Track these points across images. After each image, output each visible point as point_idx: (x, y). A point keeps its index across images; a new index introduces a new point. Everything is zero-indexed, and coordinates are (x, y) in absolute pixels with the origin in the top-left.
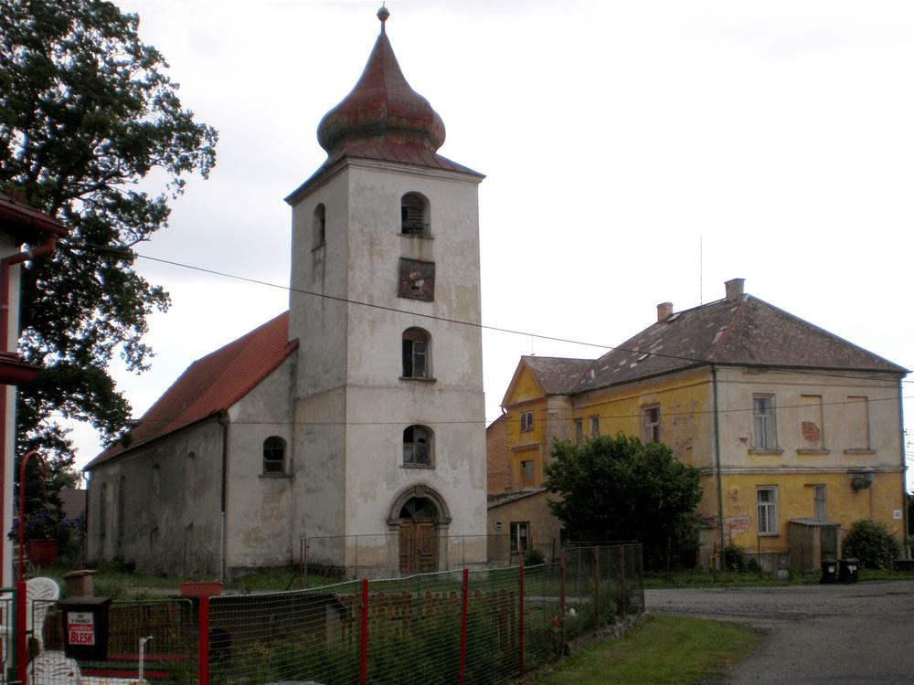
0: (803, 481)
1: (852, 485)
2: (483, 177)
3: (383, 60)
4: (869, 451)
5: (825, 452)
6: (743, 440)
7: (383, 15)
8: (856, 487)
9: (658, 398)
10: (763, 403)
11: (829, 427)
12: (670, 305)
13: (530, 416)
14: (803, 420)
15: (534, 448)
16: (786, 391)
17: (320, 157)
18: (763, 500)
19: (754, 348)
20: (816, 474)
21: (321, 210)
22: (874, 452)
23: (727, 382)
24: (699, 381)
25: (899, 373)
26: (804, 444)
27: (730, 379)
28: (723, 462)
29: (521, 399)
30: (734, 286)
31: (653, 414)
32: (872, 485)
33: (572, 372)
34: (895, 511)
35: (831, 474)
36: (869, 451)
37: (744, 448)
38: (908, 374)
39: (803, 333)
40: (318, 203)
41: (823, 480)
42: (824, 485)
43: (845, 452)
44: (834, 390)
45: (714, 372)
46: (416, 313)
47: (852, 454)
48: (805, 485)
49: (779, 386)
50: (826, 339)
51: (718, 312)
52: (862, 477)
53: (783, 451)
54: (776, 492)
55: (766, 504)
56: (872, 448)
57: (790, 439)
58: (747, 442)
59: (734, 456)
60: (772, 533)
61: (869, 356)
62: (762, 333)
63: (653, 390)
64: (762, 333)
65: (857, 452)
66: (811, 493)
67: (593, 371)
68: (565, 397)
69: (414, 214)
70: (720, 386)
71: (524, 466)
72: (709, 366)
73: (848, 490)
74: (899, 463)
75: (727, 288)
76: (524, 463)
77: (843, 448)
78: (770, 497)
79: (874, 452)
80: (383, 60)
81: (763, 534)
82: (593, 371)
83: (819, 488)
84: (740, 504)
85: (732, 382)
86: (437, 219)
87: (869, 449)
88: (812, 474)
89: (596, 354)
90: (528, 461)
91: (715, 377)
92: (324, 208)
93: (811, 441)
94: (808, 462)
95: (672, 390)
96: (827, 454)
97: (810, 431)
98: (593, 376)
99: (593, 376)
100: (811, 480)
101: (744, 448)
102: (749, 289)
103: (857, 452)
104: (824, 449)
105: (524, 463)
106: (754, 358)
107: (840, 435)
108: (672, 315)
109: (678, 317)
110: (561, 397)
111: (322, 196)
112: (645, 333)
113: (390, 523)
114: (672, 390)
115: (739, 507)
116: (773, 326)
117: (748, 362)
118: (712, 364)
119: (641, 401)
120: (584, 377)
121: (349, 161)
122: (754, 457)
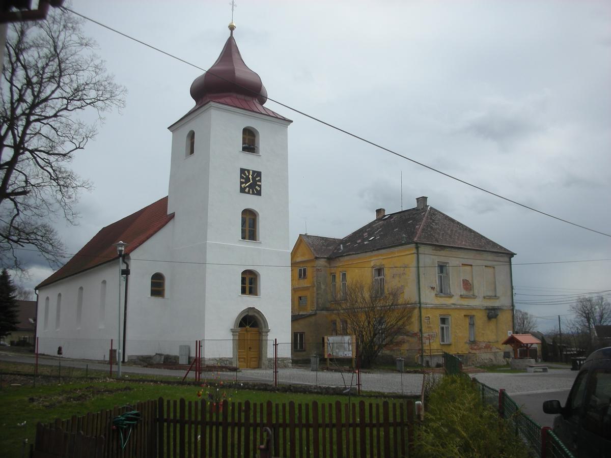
0: (463, 313)
1: (488, 316)
2: (292, 121)
3: (230, 50)
4: (496, 297)
5: (474, 297)
6: (433, 288)
7: (232, 28)
8: (490, 318)
9: (384, 262)
10: (442, 267)
11: (476, 284)
12: (384, 210)
13: (305, 270)
14: (463, 278)
15: (307, 288)
16: (454, 260)
17: (192, 103)
18: (442, 324)
19: (437, 236)
20: (470, 309)
21: (192, 135)
22: (498, 298)
23: (425, 254)
24: (408, 253)
25: (511, 255)
26: (464, 292)
27: (426, 253)
28: (422, 301)
29: (299, 259)
30: (422, 200)
31: (379, 271)
32: (498, 316)
33: (328, 245)
34: (509, 332)
35: (478, 309)
36: (496, 297)
37: (433, 293)
38: (514, 256)
39: (460, 229)
40: (190, 130)
41: (474, 313)
42: (474, 316)
43: (484, 297)
44: (478, 261)
45: (417, 248)
46: (250, 201)
47: (487, 299)
48: (465, 316)
49: (450, 258)
50: (472, 234)
51: (414, 215)
52: (493, 312)
53: (453, 295)
54: (450, 318)
55: (444, 326)
56: (497, 295)
57: (456, 288)
58: (435, 290)
59: (429, 298)
60: (448, 343)
61: (495, 245)
62: (440, 228)
63: (408, 253)
64: (440, 228)
65: (490, 298)
66: (468, 320)
67: (342, 245)
68: (325, 260)
69: (250, 142)
70: (421, 256)
71: (301, 299)
72: (414, 245)
73: (485, 318)
74: (511, 305)
75: (418, 202)
76: (300, 298)
77: (483, 295)
78: (446, 322)
79: (498, 298)
80: (230, 50)
81: (442, 343)
82: (342, 245)
83: (471, 317)
84: (431, 325)
85: (427, 254)
86: (263, 142)
87: (496, 296)
88: (468, 309)
89: (341, 237)
90: (303, 297)
91: (418, 251)
92: (194, 133)
93: (467, 291)
94: (465, 302)
95: (392, 257)
96: (475, 298)
97: (467, 285)
98: (342, 248)
99: (342, 248)
100: (467, 313)
101: (433, 293)
102: (430, 203)
103: (490, 298)
104: (474, 295)
105: (300, 298)
106: (438, 241)
107: (481, 288)
108: (385, 216)
109: (389, 217)
110: (323, 259)
111: (194, 125)
112: (370, 225)
113: (233, 331)
114: (392, 257)
115: (430, 327)
116: (444, 225)
117: (434, 243)
118: (417, 243)
119: (372, 264)
120: (336, 249)
121: (212, 108)
122: (438, 298)
